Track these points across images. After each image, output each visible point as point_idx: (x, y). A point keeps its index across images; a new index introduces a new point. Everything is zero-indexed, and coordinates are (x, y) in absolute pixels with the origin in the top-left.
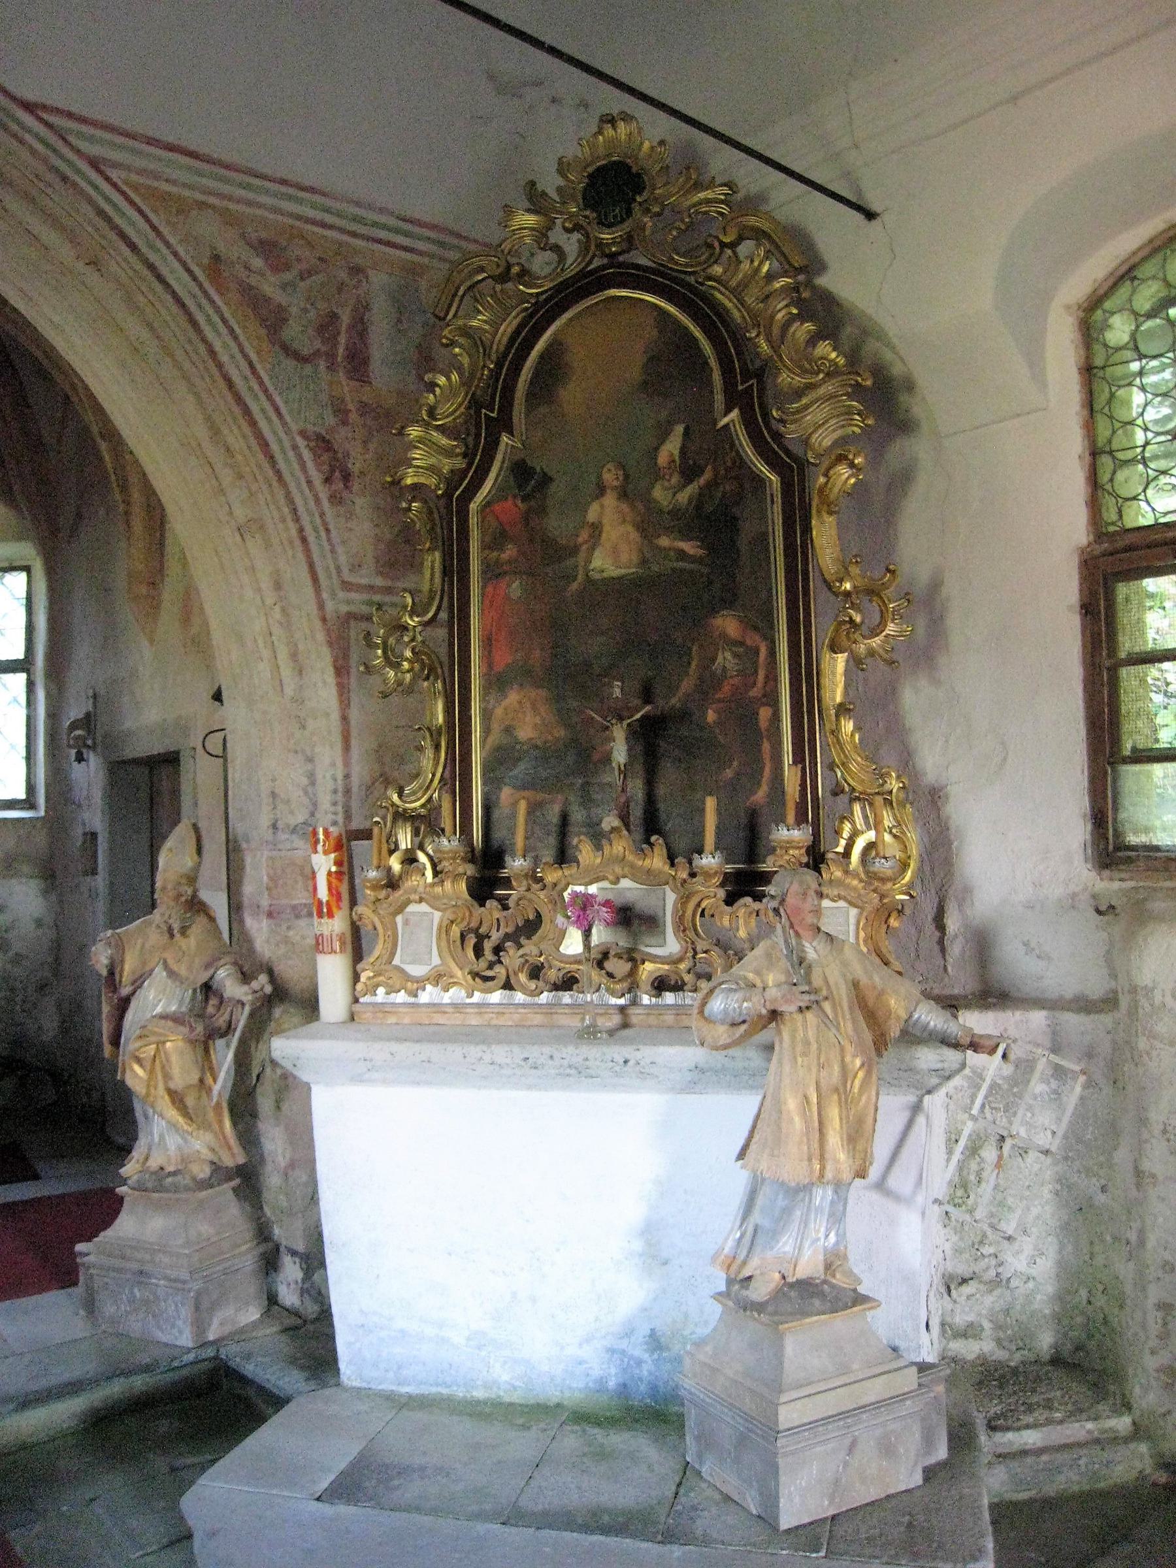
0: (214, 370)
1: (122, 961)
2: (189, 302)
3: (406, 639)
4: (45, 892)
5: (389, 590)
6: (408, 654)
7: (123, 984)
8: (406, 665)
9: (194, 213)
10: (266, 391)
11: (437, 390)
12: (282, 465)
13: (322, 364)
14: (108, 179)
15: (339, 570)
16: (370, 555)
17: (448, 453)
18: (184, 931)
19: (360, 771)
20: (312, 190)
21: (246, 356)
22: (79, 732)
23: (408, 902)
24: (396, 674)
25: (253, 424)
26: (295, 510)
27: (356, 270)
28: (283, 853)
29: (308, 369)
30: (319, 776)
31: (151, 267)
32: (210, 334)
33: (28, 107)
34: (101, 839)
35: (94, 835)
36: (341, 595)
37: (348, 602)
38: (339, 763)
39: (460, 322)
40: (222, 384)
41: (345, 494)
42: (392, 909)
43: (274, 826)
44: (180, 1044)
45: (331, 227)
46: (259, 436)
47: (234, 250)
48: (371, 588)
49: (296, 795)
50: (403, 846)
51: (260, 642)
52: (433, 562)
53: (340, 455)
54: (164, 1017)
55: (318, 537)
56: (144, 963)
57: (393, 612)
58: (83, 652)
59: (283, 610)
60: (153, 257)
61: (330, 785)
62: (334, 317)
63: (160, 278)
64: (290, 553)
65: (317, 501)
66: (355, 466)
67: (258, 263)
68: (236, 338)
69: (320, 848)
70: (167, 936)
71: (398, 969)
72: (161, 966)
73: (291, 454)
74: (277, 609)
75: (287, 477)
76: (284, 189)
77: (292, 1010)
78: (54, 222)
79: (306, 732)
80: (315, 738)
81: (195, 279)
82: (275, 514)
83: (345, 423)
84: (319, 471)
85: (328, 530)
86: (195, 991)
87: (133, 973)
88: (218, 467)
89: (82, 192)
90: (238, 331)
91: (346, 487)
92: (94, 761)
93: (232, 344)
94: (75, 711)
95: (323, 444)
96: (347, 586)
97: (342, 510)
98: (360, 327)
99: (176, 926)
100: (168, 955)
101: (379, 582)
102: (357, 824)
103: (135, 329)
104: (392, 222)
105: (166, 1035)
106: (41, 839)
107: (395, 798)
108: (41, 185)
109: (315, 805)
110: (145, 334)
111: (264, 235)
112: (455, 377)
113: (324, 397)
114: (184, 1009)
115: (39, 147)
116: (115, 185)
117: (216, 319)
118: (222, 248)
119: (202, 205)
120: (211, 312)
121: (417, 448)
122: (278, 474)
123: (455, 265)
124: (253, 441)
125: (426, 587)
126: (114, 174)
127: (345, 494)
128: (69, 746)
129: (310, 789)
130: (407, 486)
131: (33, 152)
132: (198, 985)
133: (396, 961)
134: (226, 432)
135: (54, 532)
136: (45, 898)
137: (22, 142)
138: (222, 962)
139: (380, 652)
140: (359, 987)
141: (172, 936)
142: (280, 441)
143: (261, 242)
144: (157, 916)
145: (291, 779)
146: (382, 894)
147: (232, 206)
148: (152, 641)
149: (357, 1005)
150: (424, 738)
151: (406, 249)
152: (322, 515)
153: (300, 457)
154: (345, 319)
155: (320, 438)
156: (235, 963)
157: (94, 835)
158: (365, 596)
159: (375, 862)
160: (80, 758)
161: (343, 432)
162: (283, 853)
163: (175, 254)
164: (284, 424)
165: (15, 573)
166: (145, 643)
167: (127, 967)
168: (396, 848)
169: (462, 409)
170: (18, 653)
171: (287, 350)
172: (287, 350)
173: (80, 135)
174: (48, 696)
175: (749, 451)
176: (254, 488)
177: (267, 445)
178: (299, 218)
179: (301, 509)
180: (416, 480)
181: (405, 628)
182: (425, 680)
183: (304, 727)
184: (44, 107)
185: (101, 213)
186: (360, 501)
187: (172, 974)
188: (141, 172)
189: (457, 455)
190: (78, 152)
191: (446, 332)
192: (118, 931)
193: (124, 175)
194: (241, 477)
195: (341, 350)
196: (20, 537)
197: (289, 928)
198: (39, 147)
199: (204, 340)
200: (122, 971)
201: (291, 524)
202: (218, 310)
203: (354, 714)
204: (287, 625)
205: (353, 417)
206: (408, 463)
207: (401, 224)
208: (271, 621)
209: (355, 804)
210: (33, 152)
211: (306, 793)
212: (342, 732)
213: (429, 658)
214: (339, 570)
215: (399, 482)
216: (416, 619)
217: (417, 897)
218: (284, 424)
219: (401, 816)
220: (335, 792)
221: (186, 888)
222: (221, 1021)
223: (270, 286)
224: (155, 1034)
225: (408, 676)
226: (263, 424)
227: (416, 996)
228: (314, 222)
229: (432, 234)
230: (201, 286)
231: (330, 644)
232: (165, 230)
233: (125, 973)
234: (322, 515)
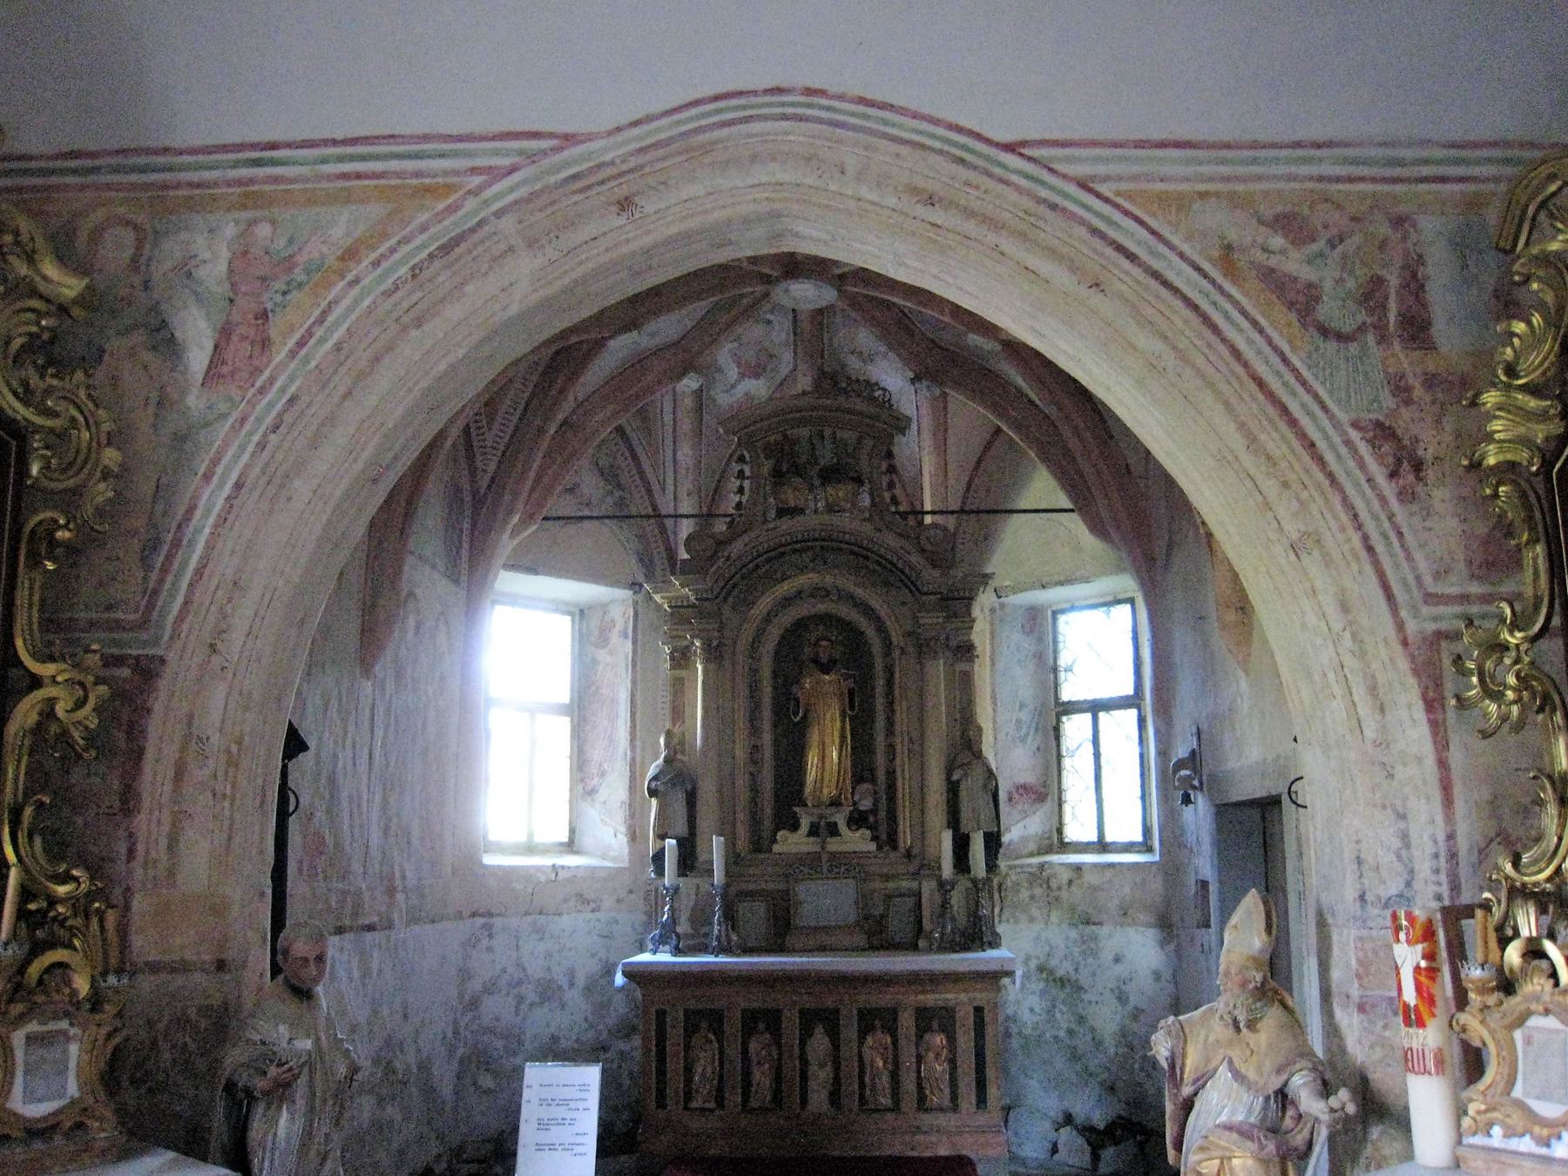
0: (1239, 369)
1: (1184, 1056)
2: (1204, 305)
3: (1507, 661)
4: (1163, 943)
5: (1488, 599)
6: (1511, 680)
7: (1185, 1081)
8: (1510, 695)
9: (1195, 206)
10: (1304, 383)
11: (1516, 341)
12: (1334, 465)
13: (1371, 339)
14: (1098, 196)
15: (1418, 579)
16: (1460, 556)
17: (1542, 416)
18: (1252, 1025)
19: (1468, 833)
20: (1330, 144)
21: (1276, 349)
22: (1184, 773)
23: (1528, 1014)
24: (1499, 706)
25: (1293, 423)
26: (1356, 516)
27: (1399, 222)
28: (1374, 933)
29: (1353, 348)
30: (1414, 835)
31: (1156, 275)
32: (1231, 333)
33: (1009, 148)
34: (1213, 888)
35: (1204, 884)
36: (1426, 610)
37: (1435, 619)
38: (1439, 819)
39: (1535, 251)
40: (1253, 386)
41: (1419, 488)
42: (1508, 1021)
43: (1362, 898)
44: (1250, 1162)
45: (1361, 179)
46: (1302, 436)
47: (1241, 230)
48: (1464, 598)
49: (1386, 858)
50: (1525, 932)
51: (1331, 675)
52: (1535, 559)
53: (1406, 442)
54: (1229, 1128)
55: (1389, 544)
56: (1208, 1060)
57: (1489, 624)
58: (1186, 687)
59: (1354, 635)
60: (1157, 265)
61: (1429, 848)
62: (1378, 281)
63: (1166, 283)
64: (1355, 567)
65: (1383, 500)
66: (1428, 451)
67: (1277, 242)
68: (1261, 331)
69: (1402, 936)
70: (1231, 1030)
71: (1520, 1105)
72: (1225, 1063)
73: (1343, 450)
74: (1347, 634)
75: (1341, 477)
76: (1300, 152)
77: (1393, 1131)
78: (1051, 253)
79: (1395, 783)
80: (1407, 790)
81: (1206, 276)
82: (1333, 524)
83: (1408, 402)
84: (1381, 464)
85: (1400, 534)
86: (1267, 1099)
87: (1197, 1069)
88: (1260, 478)
89: (1072, 216)
90: (1263, 322)
91: (1419, 479)
92: (1201, 800)
93: (1256, 336)
94: (1181, 751)
95: (1382, 433)
96: (1431, 598)
97: (1415, 507)
98: (1414, 285)
99: (1242, 1019)
100: (1236, 1054)
101: (1475, 589)
102: (1466, 898)
103: (1146, 342)
104: (1440, 153)
105: (1232, 1151)
106: (1157, 885)
107: (1508, 868)
108: (1032, 219)
109: (1412, 871)
110: (1160, 346)
111: (1280, 209)
112: (1537, 319)
113: (1378, 376)
114: (1252, 1120)
115: (1023, 182)
116: (1107, 200)
117: (1235, 314)
118: (1232, 235)
119: (1203, 195)
120: (1228, 307)
121: (1496, 417)
122: (1331, 477)
123: (1515, 181)
124: (1296, 444)
125: (1529, 591)
126: (1104, 189)
127: (1419, 488)
128: (1176, 788)
129: (1404, 852)
130: (1491, 468)
131: (1018, 188)
132: (1271, 1092)
133: (1517, 1092)
134: (1263, 437)
135: (1150, 560)
136: (1162, 948)
137: (1007, 183)
138: (1298, 1066)
139: (1475, 680)
140: (1466, 1122)
141: (1238, 1030)
142: (1327, 437)
143: (1277, 219)
144: (1220, 1004)
145: (1379, 839)
146: (1492, 999)
147: (1240, 188)
148: (1246, 672)
149: (1461, 1148)
150: (1543, 789)
151: (1462, 180)
152: (1391, 517)
153: (1354, 451)
154: (1394, 281)
155: (1379, 425)
156: (1314, 1069)
157: (1204, 884)
158: (1457, 609)
159: (1480, 957)
160: (1187, 800)
161: (1406, 414)
162: (1374, 933)
163: (1182, 255)
164: (1332, 417)
165: (1119, 607)
166: (1241, 673)
167: (1189, 1062)
168: (1517, 934)
169: (1552, 357)
170: (1129, 690)
171: (1325, 331)
172: (1325, 331)
173: (1069, 160)
174: (1157, 732)
175: (786, 588)
176: (1304, 495)
177: (1313, 445)
178: (1321, 179)
179: (1364, 515)
180: (1501, 458)
181: (1505, 647)
182: (1538, 712)
183: (1391, 776)
184: (1024, 144)
185: (1095, 232)
186: (1438, 494)
187: (1238, 1076)
188: (1134, 178)
189: (1550, 419)
190: (1065, 177)
191: (1516, 267)
192: (1181, 1018)
193: (1115, 186)
194: (1285, 485)
195: (1392, 317)
196: (1119, 570)
197: (1385, 1027)
198: (1023, 182)
199: (1224, 340)
200: (1183, 1065)
201: (1351, 532)
202: (1236, 304)
203: (1456, 757)
204: (1361, 654)
205: (1418, 392)
206: (1489, 438)
207: (1453, 153)
208: (1341, 651)
209: (1464, 871)
210: (1018, 188)
211: (1399, 857)
212: (1441, 781)
213: (1542, 684)
214: (1418, 579)
215: (1480, 464)
216: (1519, 635)
217: (1541, 1008)
218: (1332, 417)
219: (1518, 893)
220: (1436, 856)
221: (1254, 973)
222: (1299, 1139)
223: (1295, 264)
224: (1218, 1147)
225: (1515, 709)
226: (1305, 422)
227: (1548, 1145)
228: (1338, 179)
229: (1498, 153)
230: (1213, 282)
231: (1416, 672)
232: (1166, 232)
233: (1187, 1070)
234: (1391, 517)
